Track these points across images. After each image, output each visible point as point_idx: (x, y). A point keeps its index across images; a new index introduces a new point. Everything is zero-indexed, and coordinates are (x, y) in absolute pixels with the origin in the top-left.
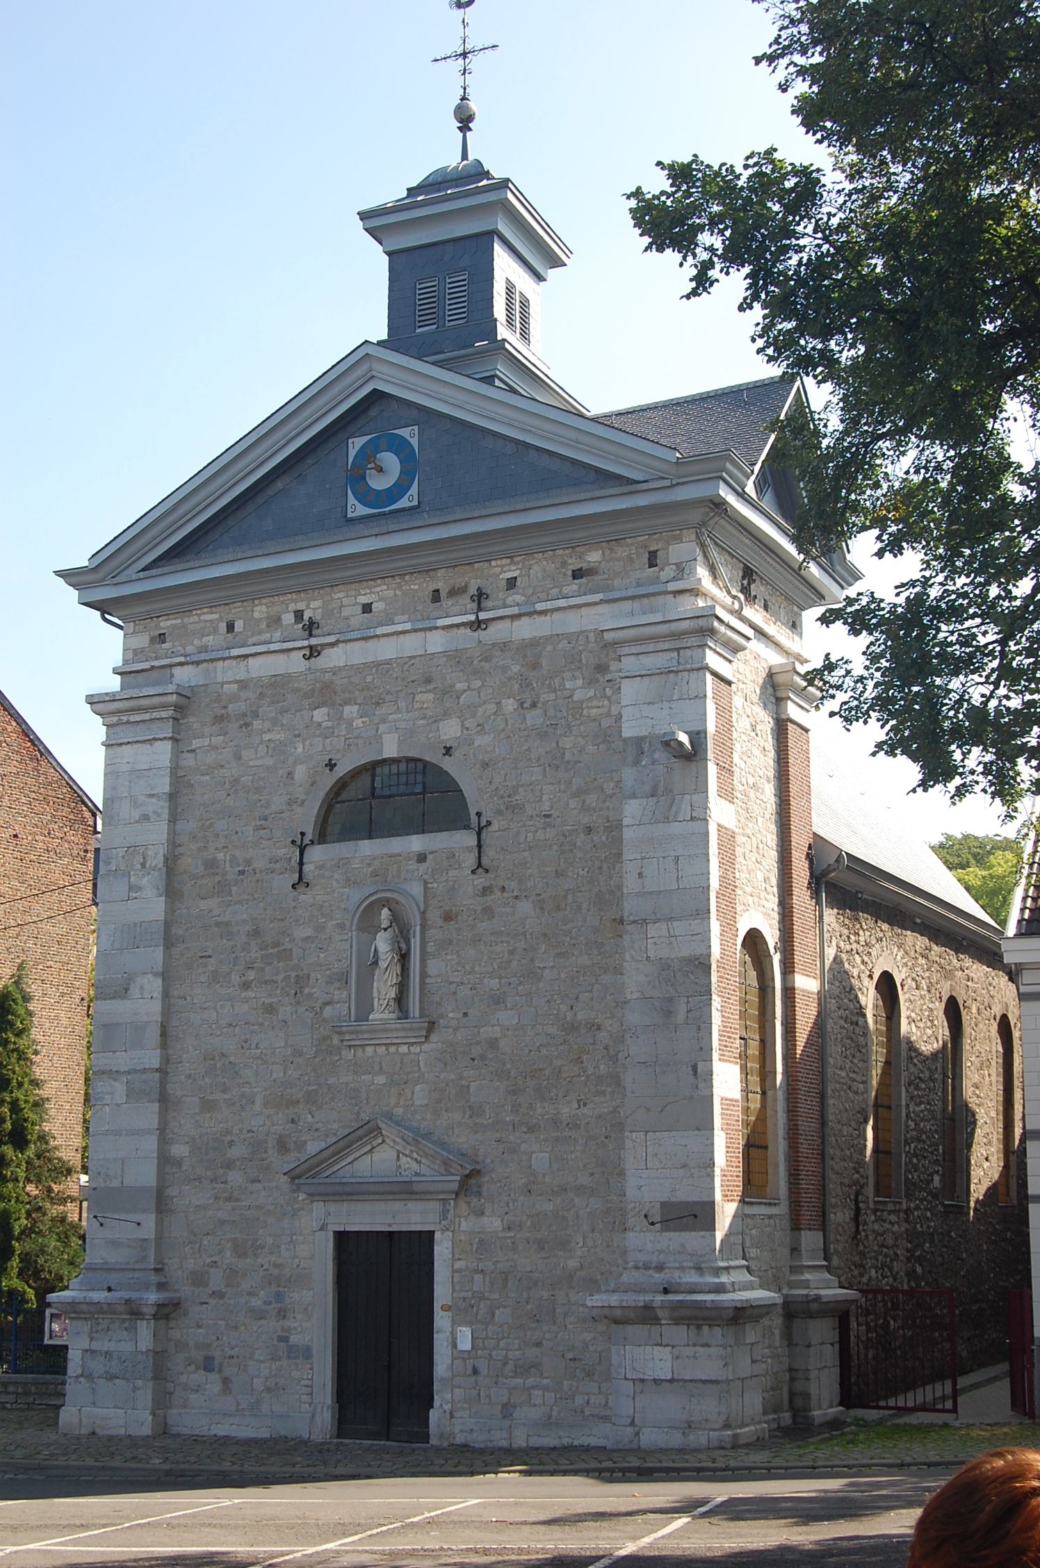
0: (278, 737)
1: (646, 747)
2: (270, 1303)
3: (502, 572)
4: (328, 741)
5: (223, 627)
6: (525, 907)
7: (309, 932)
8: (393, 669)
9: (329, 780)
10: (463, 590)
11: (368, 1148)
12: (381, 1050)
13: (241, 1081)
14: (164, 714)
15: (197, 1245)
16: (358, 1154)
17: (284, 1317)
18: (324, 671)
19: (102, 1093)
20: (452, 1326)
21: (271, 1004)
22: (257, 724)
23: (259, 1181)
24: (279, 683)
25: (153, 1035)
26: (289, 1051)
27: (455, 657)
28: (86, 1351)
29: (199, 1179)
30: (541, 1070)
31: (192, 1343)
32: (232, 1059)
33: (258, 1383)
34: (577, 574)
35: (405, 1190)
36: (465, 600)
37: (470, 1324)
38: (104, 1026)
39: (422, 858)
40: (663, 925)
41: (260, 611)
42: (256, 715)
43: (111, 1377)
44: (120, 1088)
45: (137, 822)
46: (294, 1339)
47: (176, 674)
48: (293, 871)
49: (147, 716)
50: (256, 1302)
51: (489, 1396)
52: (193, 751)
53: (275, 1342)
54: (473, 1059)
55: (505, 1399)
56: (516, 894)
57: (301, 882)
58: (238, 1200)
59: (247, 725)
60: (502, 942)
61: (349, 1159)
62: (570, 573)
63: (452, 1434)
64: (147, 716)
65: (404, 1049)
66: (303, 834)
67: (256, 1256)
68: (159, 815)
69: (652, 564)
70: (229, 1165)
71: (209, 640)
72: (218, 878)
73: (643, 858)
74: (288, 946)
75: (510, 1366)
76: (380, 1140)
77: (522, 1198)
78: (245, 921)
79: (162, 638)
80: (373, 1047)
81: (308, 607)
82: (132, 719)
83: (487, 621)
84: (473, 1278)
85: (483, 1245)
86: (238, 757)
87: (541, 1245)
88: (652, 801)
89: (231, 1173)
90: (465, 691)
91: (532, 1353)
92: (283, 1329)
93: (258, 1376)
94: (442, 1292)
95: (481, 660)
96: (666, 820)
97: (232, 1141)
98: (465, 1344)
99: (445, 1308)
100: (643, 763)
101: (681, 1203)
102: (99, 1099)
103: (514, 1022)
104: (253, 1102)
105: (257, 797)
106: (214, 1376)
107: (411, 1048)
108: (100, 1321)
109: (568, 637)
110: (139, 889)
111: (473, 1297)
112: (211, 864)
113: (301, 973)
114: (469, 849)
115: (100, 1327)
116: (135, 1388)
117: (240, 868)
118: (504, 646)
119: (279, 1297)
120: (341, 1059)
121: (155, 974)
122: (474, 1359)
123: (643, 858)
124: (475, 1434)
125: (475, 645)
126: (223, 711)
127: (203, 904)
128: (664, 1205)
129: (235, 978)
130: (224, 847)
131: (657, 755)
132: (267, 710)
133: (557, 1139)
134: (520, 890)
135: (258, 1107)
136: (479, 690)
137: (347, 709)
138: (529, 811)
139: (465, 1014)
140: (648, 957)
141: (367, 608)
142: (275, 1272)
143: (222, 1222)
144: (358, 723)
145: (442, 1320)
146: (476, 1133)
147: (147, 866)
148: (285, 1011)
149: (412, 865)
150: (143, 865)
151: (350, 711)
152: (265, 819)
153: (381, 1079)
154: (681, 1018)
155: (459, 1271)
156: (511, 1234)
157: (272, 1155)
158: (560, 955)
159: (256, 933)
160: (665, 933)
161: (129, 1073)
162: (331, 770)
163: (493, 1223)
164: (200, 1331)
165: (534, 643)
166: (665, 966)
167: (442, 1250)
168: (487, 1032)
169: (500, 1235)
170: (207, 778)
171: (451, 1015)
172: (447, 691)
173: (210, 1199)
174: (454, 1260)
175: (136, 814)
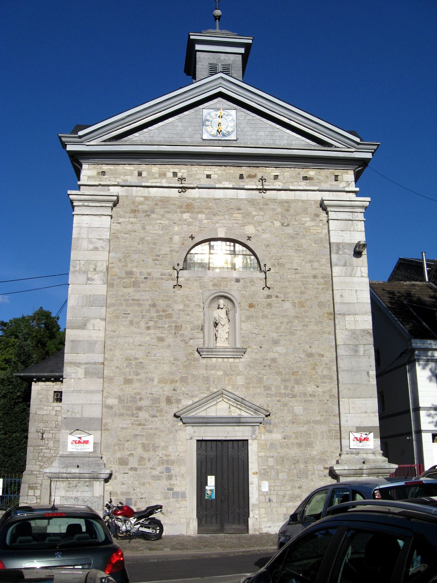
0: (165, 222)
1: (341, 247)
2: (163, 473)
3: (272, 172)
4: (190, 227)
5: (136, 173)
6: (288, 305)
7: (181, 307)
8: (222, 202)
10: (254, 176)
11: (215, 402)
13: (146, 371)
14: (107, 205)
15: (122, 446)
16: (209, 405)
17: (171, 479)
18: (188, 198)
19: (70, 372)
20: (259, 481)
21: (162, 337)
22: (153, 216)
23: (157, 417)
24: (165, 201)
25: (99, 347)
26: (172, 359)
27: (252, 202)
28: (63, 497)
29: (122, 415)
30: (297, 372)
31: (119, 493)
32: (141, 360)
34: (305, 178)
35: (238, 422)
36: (256, 180)
37: (267, 480)
38: (72, 341)
40: (352, 316)
42: (153, 212)
44: (81, 372)
45: (91, 250)
46: (176, 489)
47: (111, 189)
49: (98, 204)
50: (155, 473)
52: (120, 223)
53: (166, 491)
54: (265, 366)
56: (283, 299)
58: (144, 425)
59: (149, 216)
60: (277, 318)
61: (205, 408)
62: (302, 178)
63: (260, 528)
64: (98, 204)
67: (155, 451)
68: (103, 248)
69: (336, 181)
70: (140, 409)
71: (129, 178)
72: (133, 280)
73: (343, 289)
74: (170, 312)
75: (287, 497)
76: (221, 399)
77: (290, 425)
78: (148, 300)
79: (103, 173)
81: (180, 171)
82: (90, 204)
83: (266, 190)
84: (268, 460)
85: (273, 446)
86: (144, 228)
87: (300, 445)
90: (256, 215)
92: (171, 485)
94: (253, 466)
95: (263, 205)
96: (351, 276)
97: (141, 398)
100: (340, 253)
101: (365, 427)
102: (69, 375)
103: (284, 351)
104: (153, 381)
105: (154, 246)
107: (235, 360)
108: (71, 482)
109: (303, 201)
110: (93, 280)
111: (268, 468)
112: (130, 273)
113: (178, 324)
114: (261, 279)
115: (71, 485)
117: (145, 276)
118: (274, 201)
119: (168, 470)
121: (102, 319)
122: (269, 495)
123: (343, 289)
124: (272, 528)
125: (260, 198)
126: (136, 208)
127: (125, 290)
129: (143, 324)
130: (136, 266)
131: (346, 251)
132: (158, 210)
133: (305, 401)
134: (285, 298)
135: (156, 382)
136: (263, 216)
137: (200, 216)
138: (288, 267)
139: (261, 347)
140: (346, 329)
141: (208, 176)
142: (165, 458)
143: (136, 436)
144: (205, 221)
145: (253, 479)
146: (267, 397)
147: (97, 270)
148: (170, 340)
149: (233, 283)
150: (95, 269)
151: (201, 216)
152: (158, 256)
153: (221, 373)
154: (361, 353)
155: (262, 457)
156: (286, 441)
157: (163, 404)
158: (304, 325)
159: (154, 305)
160: (353, 319)
161: (86, 364)
162: (192, 239)
164: (123, 486)
165: (287, 202)
166: (353, 332)
167: (253, 448)
168: (271, 355)
170: (128, 235)
171: (254, 347)
172: (248, 214)
173: (129, 424)
174: (258, 452)
175: (91, 247)
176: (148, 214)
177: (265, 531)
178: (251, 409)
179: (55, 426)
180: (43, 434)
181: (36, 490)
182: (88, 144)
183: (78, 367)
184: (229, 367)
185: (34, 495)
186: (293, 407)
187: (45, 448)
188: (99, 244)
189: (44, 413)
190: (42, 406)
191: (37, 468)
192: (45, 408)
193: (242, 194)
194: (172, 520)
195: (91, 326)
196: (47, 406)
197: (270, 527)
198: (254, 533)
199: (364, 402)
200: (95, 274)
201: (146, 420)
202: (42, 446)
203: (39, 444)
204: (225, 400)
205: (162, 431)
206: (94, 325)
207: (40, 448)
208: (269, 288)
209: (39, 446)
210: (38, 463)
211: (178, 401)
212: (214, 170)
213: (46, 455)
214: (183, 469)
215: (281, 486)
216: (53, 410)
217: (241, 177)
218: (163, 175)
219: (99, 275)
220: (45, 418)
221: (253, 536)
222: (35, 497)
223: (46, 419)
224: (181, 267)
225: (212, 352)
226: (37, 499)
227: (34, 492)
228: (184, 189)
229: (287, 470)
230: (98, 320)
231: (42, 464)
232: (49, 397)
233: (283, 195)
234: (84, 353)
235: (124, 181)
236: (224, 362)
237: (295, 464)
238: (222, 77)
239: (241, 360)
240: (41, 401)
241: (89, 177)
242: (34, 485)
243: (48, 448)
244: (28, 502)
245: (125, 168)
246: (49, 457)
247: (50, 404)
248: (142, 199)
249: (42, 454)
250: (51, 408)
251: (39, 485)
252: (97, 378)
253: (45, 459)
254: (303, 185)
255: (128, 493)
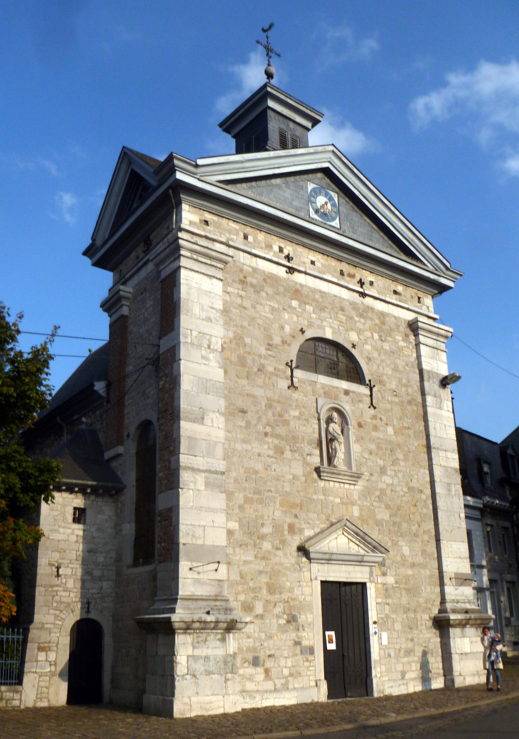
9: (348, 346)
12: (337, 485)
19: (188, 481)
25: (219, 451)
27: (353, 305)
28: (190, 656)
33: (286, 672)
34: (395, 292)
35: (360, 561)
38: (188, 437)
39: (347, 393)
40: (444, 452)
41: (261, 236)
43: (209, 673)
44: (201, 479)
46: (305, 643)
48: (287, 378)
49: (209, 262)
51: (395, 668)
55: (402, 669)
57: (292, 386)
64: (209, 262)
65: (347, 486)
66: (292, 361)
68: (217, 321)
70: (262, 537)
75: (402, 652)
79: (206, 223)
80: (333, 483)
82: (201, 259)
86: (254, 307)
88: (435, 399)
89: (265, 543)
91: (410, 645)
93: (286, 667)
94: (373, 615)
98: (385, 642)
99: (375, 623)
102: (186, 485)
106: (260, 670)
114: (366, 395)
115: (200, 639)
116: (226, 680)
120: (318, 486)
124: (394, 688)
128: (456, 574)
137: (308, 307)
141: (313, 263)
145: (372, 628)
160: (444, 455)
163: (390, 580)
164: (249, 640)
169: (394, 585)
175: (204, 315)
176: (258, 289)
177: (387, 692)
178: (370, 546)
179: (75, 558)
180: (58, 568)
181: (49, 653)
182: (202, 178)
183: (197, 474)
184: (345, 495)
185: (47, 660)
186: (402, 546)
187: (62, 589)
188: (213, 314)
189: (61, 537)
190: (57, 527)
191: (51, 618)
192: (62, 530)
193: (345, 294)
194: (302, 683)
195: (209, 421)
196: (64, 527)
197: (392, 687)
198: (379, 695)
199: (458, 546)
200: (210, 353)
201: (269, 552)
202: (58, 586)
203: (53, 584)
204: (345, 533)
205: (286, 568)
206: (212, 421)
207: (55, 589)
208: (375, 408)
209: (53, 586)
210: (51, 611)
211: (301, 531)
212: (317, 256)
213: (63, 600)
214: (310, 618)
215: (397, 638)
216: (72, 534)
217: (342, 273)
218: (269, 247)
219: (214, 355)
220: (62, 546)
221: (379, 699)
222: (48, 663)
223: (63, 547)
224: (294, 365)
225: (338, 474)
226: (51, 665)
227: (47, 655)
228: (291, 270)
229: (401, 620)
230: (217, 414)
231: (58, 612)
232: (67, 514)
233: (379, 306)
234: (203, 457)
235: (229, 239)
236: (340, 487)
237: (406, 612)
238: (333, 152)
239: (356, 487)
240: (55, 520)
241: (191, 223)
242: (46, 645)
243: (66, 589)
244: (37, 671)
245: (229, 224)
246: (67, 603)
247: (69, 526)
248: (250, 269)
249: (57, 598)
250: (69, 531)
251: (55, 645)
252: (219, 492)
253: (62, 607)
254: (393, 299)
255: (255, 649)
